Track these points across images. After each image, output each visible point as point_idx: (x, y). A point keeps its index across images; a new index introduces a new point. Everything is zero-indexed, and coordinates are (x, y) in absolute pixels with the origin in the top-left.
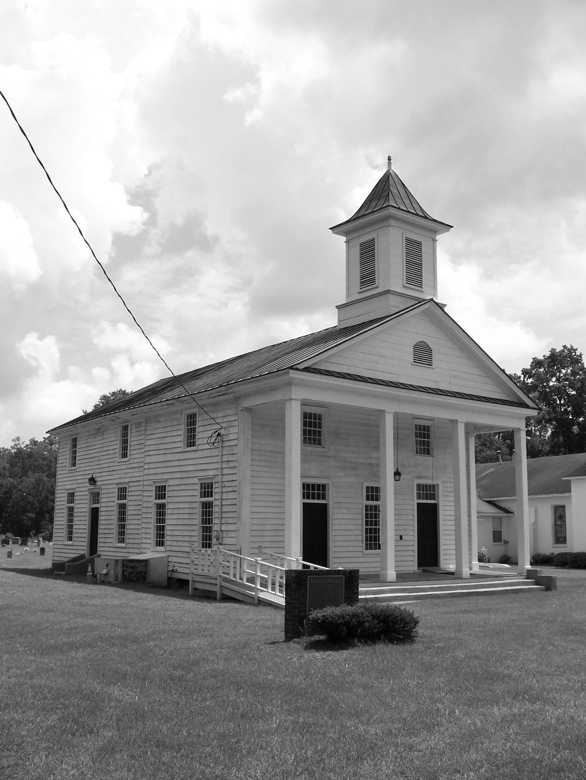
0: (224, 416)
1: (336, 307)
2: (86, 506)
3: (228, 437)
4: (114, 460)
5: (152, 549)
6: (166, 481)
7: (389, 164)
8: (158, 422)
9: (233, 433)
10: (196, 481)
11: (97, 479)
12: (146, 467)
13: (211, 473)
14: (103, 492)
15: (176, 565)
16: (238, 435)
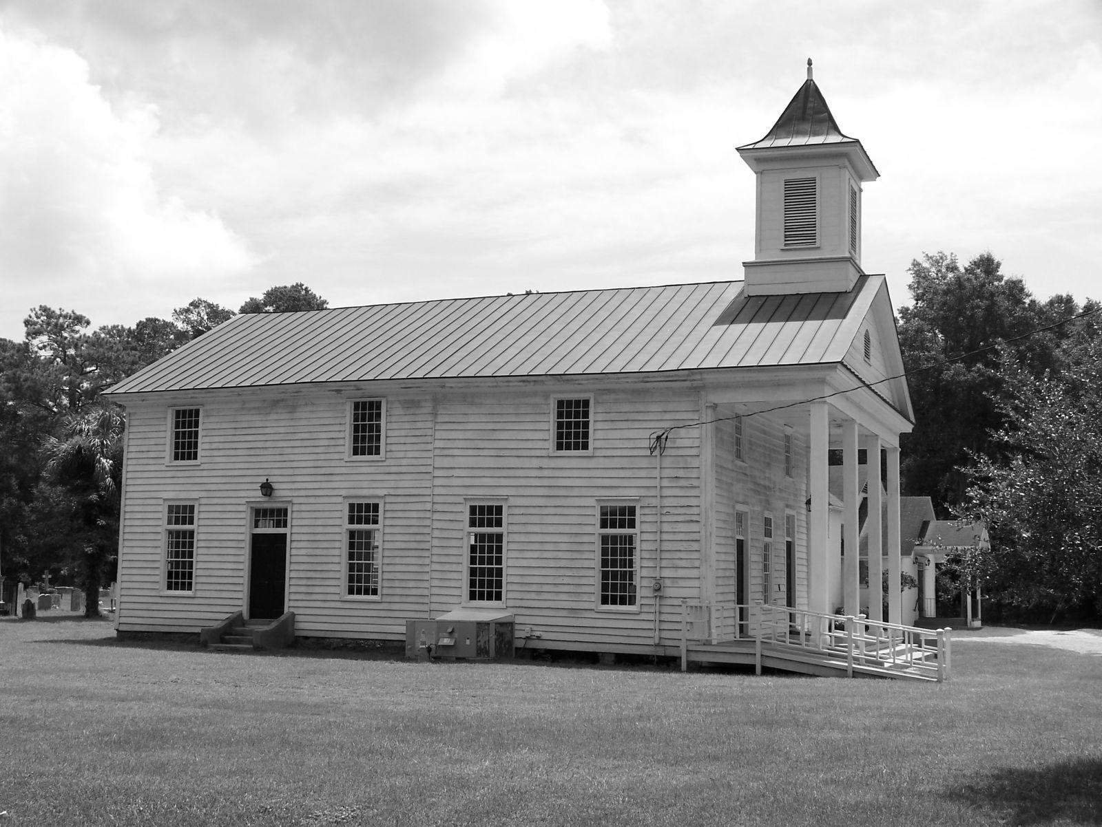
0: (665, 412)
1: (743, 263)
2: (242, 530)
3: (675, 442)
4: (341, 456)
5: (463, 604)
6: (507, 499)
7: (810, 71)
8: (472, 404)
9: (686, 439)
10: (592, 502)
11: (275, 486)
12: (437, 473)
13: (634, 493)
14: (296, 508)
15: (535, 628)
16: (701, 442)
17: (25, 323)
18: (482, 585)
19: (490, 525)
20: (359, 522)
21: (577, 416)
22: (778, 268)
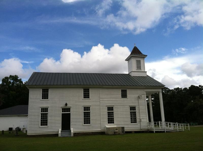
10: (128, 106)
17: (155, 69)
18: (110, 121)
19: (111, 110)
20: (86, 110)
21: (46, 92)
22: (138, 72)
